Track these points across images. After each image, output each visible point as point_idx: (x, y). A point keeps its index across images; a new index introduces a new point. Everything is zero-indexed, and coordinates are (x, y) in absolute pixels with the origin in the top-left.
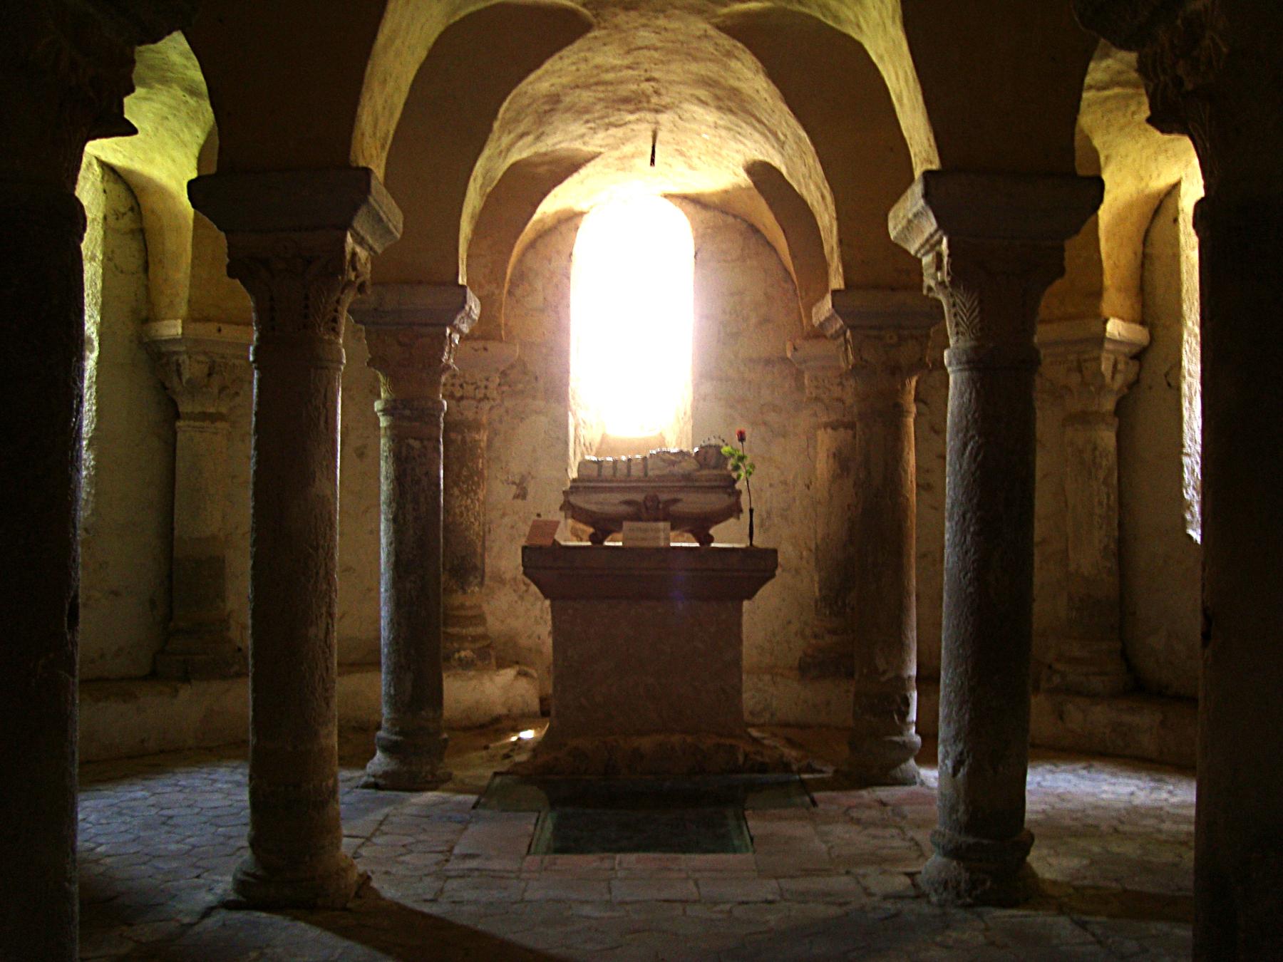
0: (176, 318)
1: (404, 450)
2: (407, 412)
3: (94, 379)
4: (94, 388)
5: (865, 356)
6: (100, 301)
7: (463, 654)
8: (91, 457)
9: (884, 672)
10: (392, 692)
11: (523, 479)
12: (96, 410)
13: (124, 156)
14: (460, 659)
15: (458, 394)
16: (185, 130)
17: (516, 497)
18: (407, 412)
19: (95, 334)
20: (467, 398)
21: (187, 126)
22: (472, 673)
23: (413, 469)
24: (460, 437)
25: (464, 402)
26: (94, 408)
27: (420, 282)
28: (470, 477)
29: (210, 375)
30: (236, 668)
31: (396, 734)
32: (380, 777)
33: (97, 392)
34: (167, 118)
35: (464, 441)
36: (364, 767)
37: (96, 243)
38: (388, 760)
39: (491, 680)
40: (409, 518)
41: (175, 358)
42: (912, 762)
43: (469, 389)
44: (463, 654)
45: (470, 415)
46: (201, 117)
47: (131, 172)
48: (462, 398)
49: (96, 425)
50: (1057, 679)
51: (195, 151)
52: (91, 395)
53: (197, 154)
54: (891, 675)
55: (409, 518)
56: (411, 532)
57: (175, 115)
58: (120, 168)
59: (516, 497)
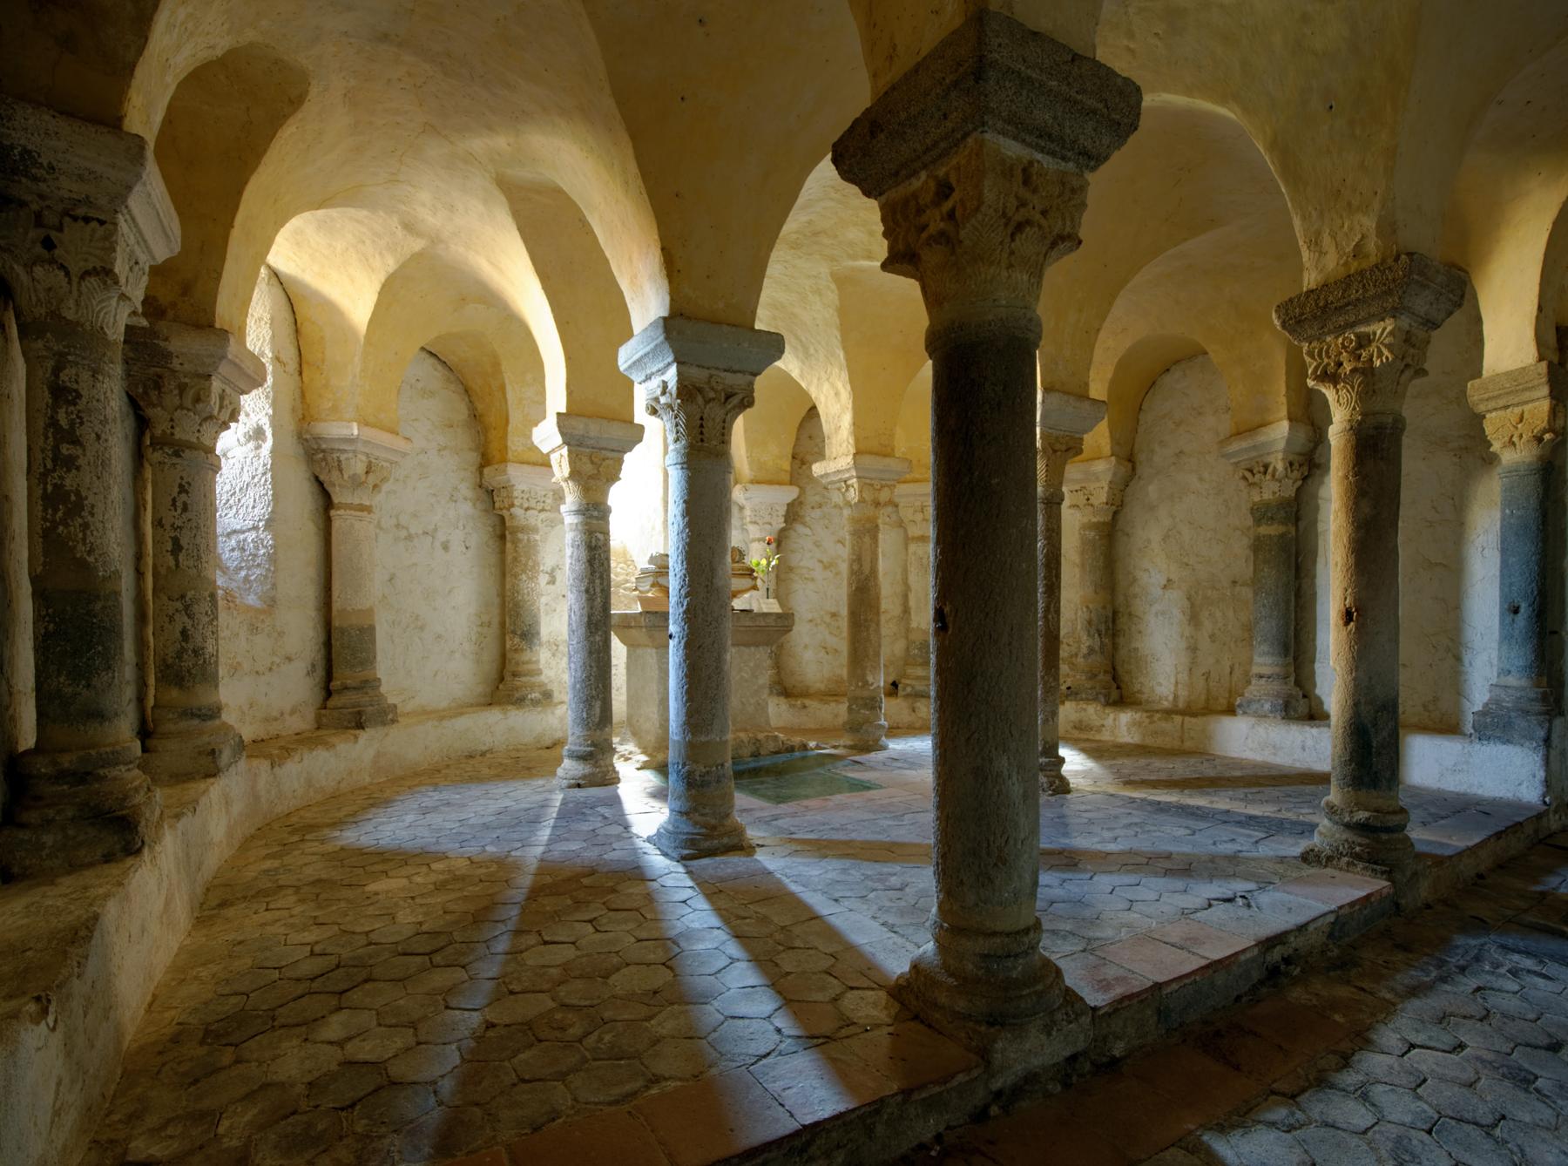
0: (1281, 419)
1: (593, 540)
2: (596, 513)
3: (269, 467)
4: (269, 475)
5: (864, 495)
6: (271, 395)
7: (533, 695)
8: (269, 537)
9: (872, 684)
10: (585, 715)
11: (553, 570)
12: (273, 495)
13: (297, 265)
14: (532, 700)
15: (526, 505)
16: (377, 256)
17: (548, 583)
18: (596, 513)
19: (268, 425)
20: (533, 509)
21: (380, 254)
22: (540, 709)
23: (600, 555)
24: (526, 537)
25: (529, 512)
26: (270, 493)
27: (613, 420)
28: (534, 567)
29: (367, 473)
30: (390, 717)
31: (588, 746)
32: (580, 778)
33: (272, 478)
34: (364, 242)
35: (529, 540)
36: (554, 774)
37: (264, 341)
38: (582, 766)
39: (553, 713)
40: (598, 590)
41: (335, 456)
42: (883, 738)
43: (532, 503)
44: (533, 695)
45: (532, 521)
46: (399, 250)
47: (295, 281)
48: (527, 509)
49: (274, 507)
50: (909, 689)
51: (382, 277)
52: (266, 481)
53: (383, 280)
54: (875, 685)
55: (598, 590)
56: (599, 600)
57: (374, 241)
58: (286, 275)
59: (548, 583)
